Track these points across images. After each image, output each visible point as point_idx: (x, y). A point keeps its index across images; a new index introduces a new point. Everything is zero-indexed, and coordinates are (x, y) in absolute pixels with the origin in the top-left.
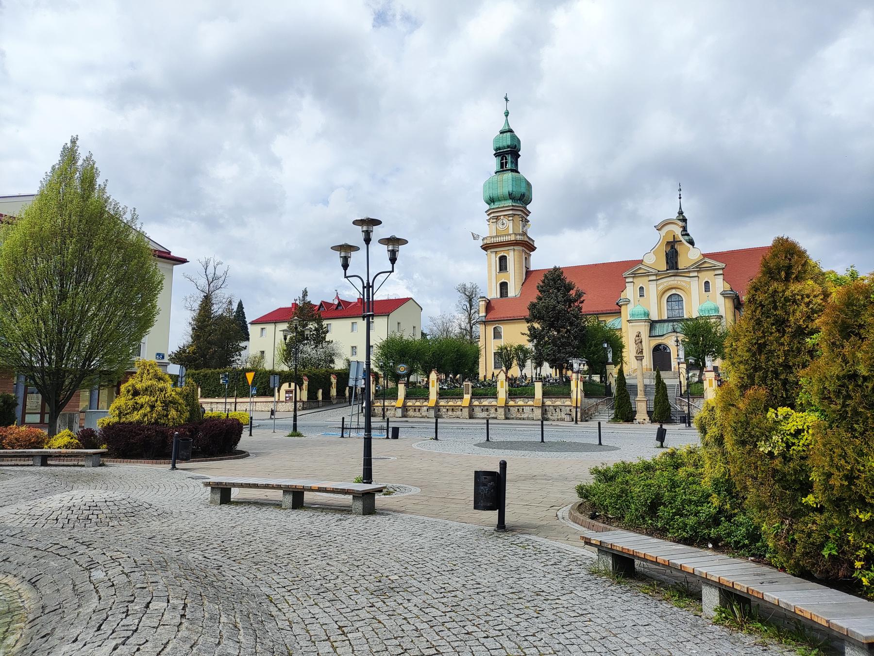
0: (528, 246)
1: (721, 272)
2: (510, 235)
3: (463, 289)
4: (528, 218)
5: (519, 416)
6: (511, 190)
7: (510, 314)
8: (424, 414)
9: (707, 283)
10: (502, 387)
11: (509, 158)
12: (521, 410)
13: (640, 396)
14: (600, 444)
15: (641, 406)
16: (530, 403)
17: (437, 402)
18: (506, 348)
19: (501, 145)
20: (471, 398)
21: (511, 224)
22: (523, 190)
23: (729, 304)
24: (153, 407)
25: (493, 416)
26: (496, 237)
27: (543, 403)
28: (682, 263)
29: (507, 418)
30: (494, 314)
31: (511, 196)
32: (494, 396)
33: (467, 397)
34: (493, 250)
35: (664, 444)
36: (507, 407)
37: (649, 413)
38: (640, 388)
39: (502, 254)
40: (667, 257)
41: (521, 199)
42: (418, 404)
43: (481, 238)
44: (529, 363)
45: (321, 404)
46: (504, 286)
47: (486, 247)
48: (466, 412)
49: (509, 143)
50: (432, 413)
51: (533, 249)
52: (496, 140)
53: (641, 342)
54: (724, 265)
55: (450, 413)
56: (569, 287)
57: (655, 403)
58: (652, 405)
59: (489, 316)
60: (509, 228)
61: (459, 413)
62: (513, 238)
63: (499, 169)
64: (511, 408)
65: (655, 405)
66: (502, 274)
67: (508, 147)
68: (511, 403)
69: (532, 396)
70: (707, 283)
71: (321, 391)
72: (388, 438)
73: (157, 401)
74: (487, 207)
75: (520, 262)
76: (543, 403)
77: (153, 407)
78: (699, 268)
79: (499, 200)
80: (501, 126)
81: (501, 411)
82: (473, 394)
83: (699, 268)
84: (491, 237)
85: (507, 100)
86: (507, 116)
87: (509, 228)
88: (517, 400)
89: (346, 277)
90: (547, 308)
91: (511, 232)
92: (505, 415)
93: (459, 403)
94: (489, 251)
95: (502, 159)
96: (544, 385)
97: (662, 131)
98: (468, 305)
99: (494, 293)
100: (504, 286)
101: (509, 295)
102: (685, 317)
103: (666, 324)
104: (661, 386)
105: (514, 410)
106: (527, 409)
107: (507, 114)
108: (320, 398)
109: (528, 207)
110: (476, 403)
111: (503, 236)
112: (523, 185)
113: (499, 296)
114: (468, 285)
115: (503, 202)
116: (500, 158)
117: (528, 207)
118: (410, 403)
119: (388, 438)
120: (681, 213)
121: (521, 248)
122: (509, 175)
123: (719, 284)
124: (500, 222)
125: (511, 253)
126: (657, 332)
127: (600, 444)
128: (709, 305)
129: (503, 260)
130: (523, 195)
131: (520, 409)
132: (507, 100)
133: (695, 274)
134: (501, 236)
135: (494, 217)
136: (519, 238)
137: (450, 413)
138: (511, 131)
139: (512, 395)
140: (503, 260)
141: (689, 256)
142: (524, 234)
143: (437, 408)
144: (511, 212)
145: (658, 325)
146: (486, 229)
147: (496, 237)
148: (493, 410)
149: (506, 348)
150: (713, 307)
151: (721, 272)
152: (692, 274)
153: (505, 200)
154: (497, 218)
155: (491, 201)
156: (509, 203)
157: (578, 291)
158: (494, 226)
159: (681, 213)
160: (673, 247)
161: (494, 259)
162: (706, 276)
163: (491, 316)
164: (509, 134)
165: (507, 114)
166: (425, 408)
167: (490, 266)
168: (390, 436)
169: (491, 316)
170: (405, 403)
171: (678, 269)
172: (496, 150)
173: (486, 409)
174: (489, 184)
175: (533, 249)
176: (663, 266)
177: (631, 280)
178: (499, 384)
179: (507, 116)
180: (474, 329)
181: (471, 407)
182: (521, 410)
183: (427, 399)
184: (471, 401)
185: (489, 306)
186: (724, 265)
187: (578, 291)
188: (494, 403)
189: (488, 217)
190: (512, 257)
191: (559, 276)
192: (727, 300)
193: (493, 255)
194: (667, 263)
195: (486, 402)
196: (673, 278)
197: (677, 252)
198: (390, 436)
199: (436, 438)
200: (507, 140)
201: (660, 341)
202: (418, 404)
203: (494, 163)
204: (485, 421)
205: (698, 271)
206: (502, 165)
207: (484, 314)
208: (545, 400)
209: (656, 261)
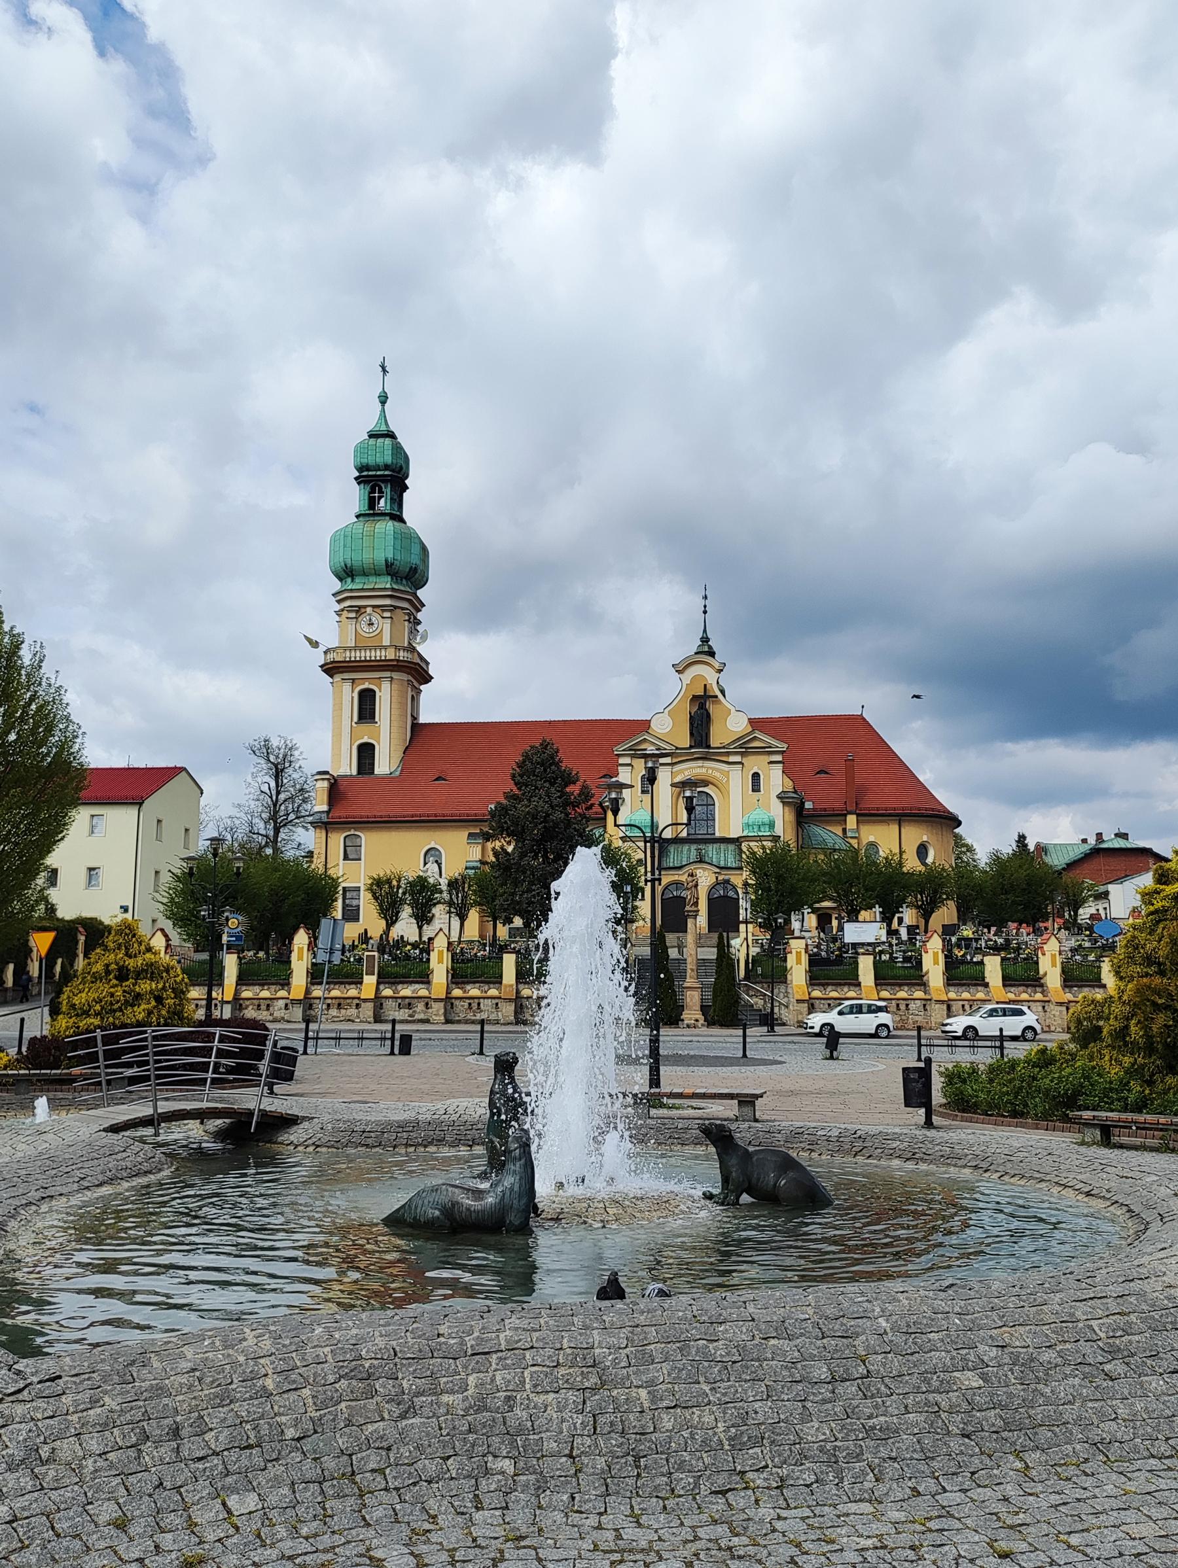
0: (419, 673)
1: (779, 758)
2: (385, 648)
3: (265, 749)
4: (419, 616)
5: (470, 1016)
6: (390, 556)
7: (381, 811)
8: (277, 1014)
9: (756, 776)
10: (440, 961)
11: (387, 490)
12: (475, 1006)
13: (690, 981)
14: (745, 1055)
15: (692, 1000)
16: (493, 992)
17: (308, 991)
18: (389, 881)
19: (371, 461)
20: (378, 983)
21: (387, 626)
22: (415, 560)
23: (790, 816)
24: (159, 1000)
25: (422, 1016)
26: (356, 648)
27: (518, 992)
28: (718, 737)
29: (448, 1021)
30: (350, 805)
31: (390, 569)
32: (424, 978)
33: (370, 980)
34: (346, 676)
35: (835, 1054)
36: (448, 1000)
37: (704, 1009)
38: (690, 965)
39: (366, 685)
40: (691, 724)
41: (407, 575)
42: (265, 994)
43: (322, 648)
44: (439, 911)
45: (10, 994)
46: (366, 752)
47: (331, 669)
48: (368, 1010)
49: (388, 459)
50: (298, 1012)
51: (426, 678)
52: (360, 449)
53: (696, 886)
54: (783, 746)
55: (334, 1012)
56: (569, 779)
57: (714, 992)
58: (709, 995)
59: (336, 813)
60: (383, 632)
61: (352, 1012)
62: (390, 654)
63: (365, 509)
64: (457, 1002)
65: (715, 996)
66: (366, 727)
67: (386, 467)
68: (457, 992)
69: (497, 980)
70: (756, 776)
71: (11, 967)
72: (392, 1053)
73: (164, 988)
74: (337, 585)
75: (403, 705)
76: (518, 992)
77: (159, 1000)
78: (744, 747)
79: (365, 573)
80: (371, 423)
81: (438, 1009)
82: (379, 977)
83: (744, 747)
84: (345, 649)
85: (384, 370)
86: (383, 403)
87: (383, 632)
88: (468, 987)
89: (616, 825)
90: (534, 817)
91: (386, 641)
92: (445, 1014)
93: (353, 992)
94: (338, 678)
95: (372, 491)
96: (517, 958)
97: (636, 454)
98: (273, 784)
99: (347, 766)
100: (366, 752)
101: (376, 772)
102: (718, 834)
103: (686, 848)
104: (725, 960)
105: (461, 1006)
106: (486, 1004)
107: (383, 399)
108: (10, 982)
109: (419, 593)
110: (387, 992)
111: (370, 648)
112: (416, 549)
113: (354, 772)
114: (275, 742)
115: (373, 579)
116: (368, 488)
117: (419, 593)
118: (246, 994)
119: (392, 1053)
120: (705, 640)
121: (405, 677)
122: (387, 527)
123: (776, 780)
124: (364, 619)
125: (386, 686)
126: (672, 861)
127: (745, 1055)
128: (759, 815)
129: (367, 702)
130: (414, 570)
131: (474, 1003)
132: (384, 370)
133: (738, 758)
134: (365, 648)
135: (352, 607)
136: (402, 655)
137: (334, 1012)
138: (391, 435)
139: (458, 976)
140: (367, 702)
141: (730, 725)
142: (412, 649)
143: (307, 1002)
144: (388, 602)
145: (672, 848)
146: (331, 632)
147: (356, 648)
148: (420, 1006)
149: (389, 881)
150: (766, 820)
151: (779, 758)
152: (732, 759)
153: (377, 574)
154: (359, 610)
155: (346, 573)
156: (386, 582)
157: (585, 787)
158: (351, 627)
159: (705, 640)
160: (702, 706)
161: (349, 695)
162: (756, 763)
163: (340, 813)
164: (388, 441)
165: (383, 399)
166: (281, 1003)
167: (338, 707)
168: (396, 1051)
169: (340, 813)
170: (237, 992)
171: (709, 747)
172: (361, 469)
173: (407, 1003)
174: (342, 538)
175: (426, 678)
176: (684, 741)
177: (627, 760)
178: (434, 956)
179: (383, 403)
180: (282, 835)
181: (378, 1001)
182: (475, 1006)
183: (285, 983)
184: (377, 989)
185: (336, 790)
186: (783, 746)
187: (585, 787)
188: (423, 992)
189: (338, 607)
190: (386, 695)
191: (552, 757)
192: (787, 809)
193: (347, 686)
194: (692, 734)
195: (406, 991)
196: (700, 763)
197: (708, 716)
198: (396, 1051)
199: (481, 1053)
200: (383, 454)
201: (676, 878)
202: (265, 994)
203: (354, 497)
204: (478, 1028)
205: (742, 754)
206: (372, 503)
207: (325, 808)
208: (521, 987)
209: (669, 728)
